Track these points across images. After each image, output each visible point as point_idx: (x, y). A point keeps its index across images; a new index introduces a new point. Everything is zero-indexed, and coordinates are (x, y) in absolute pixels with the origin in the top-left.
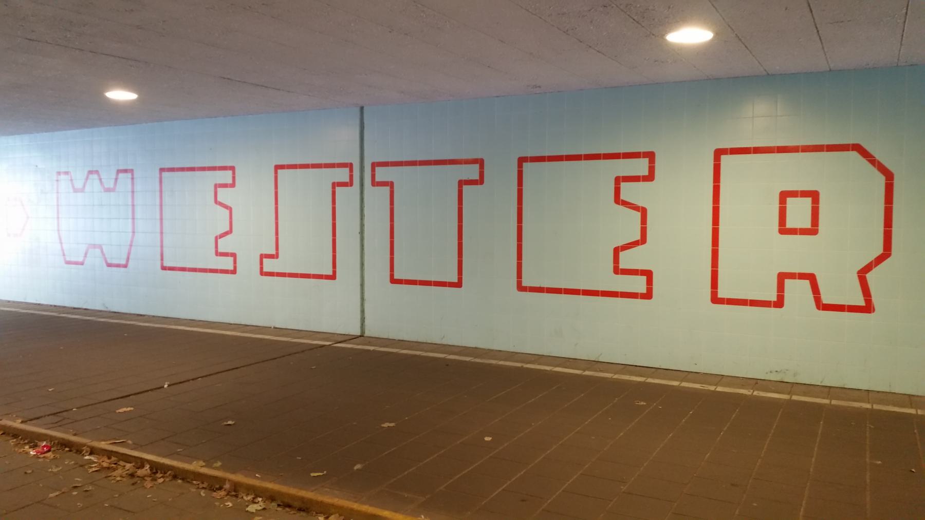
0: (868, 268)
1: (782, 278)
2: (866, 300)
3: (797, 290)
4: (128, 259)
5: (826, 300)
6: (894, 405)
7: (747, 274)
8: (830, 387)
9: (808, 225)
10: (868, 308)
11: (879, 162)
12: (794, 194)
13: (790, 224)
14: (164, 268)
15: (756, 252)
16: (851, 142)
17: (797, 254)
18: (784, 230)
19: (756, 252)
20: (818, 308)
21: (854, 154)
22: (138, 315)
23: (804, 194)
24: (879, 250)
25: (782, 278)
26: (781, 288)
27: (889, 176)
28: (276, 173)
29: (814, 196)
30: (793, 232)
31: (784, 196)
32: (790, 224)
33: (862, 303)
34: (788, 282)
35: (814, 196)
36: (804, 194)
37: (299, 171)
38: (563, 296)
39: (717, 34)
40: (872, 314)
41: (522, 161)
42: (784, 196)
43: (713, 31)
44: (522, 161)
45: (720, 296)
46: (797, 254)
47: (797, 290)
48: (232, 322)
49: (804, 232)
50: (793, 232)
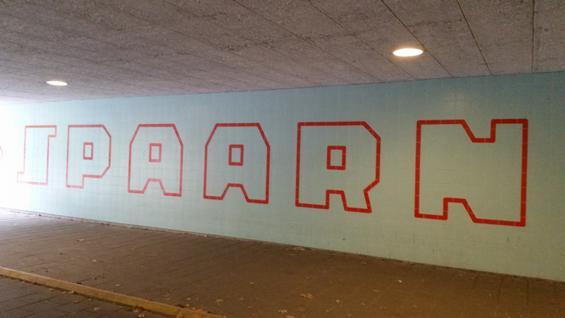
0: (368, 188)
1: (446, 201)
3: (335, 199)
4: (181, 189)
5: (349, 205)
7: (313, 193)
10: (369, 210)
13: (332, 164)
14: (130, 191)
16: (361, 120)
18: (330, 167)
20: (345, 210)
22: (447, 267)
25: (446, 201)
28: (69, 129)
31: (330, 148)
32: (332, 164)
33: (365, 207)
34: (450, 204)
38: (313, 209)
39: (391, 54)
41: (420, 123)
42: (330, 148)
43: (394, 55)
44: (300, 125)
47: (335, 199)
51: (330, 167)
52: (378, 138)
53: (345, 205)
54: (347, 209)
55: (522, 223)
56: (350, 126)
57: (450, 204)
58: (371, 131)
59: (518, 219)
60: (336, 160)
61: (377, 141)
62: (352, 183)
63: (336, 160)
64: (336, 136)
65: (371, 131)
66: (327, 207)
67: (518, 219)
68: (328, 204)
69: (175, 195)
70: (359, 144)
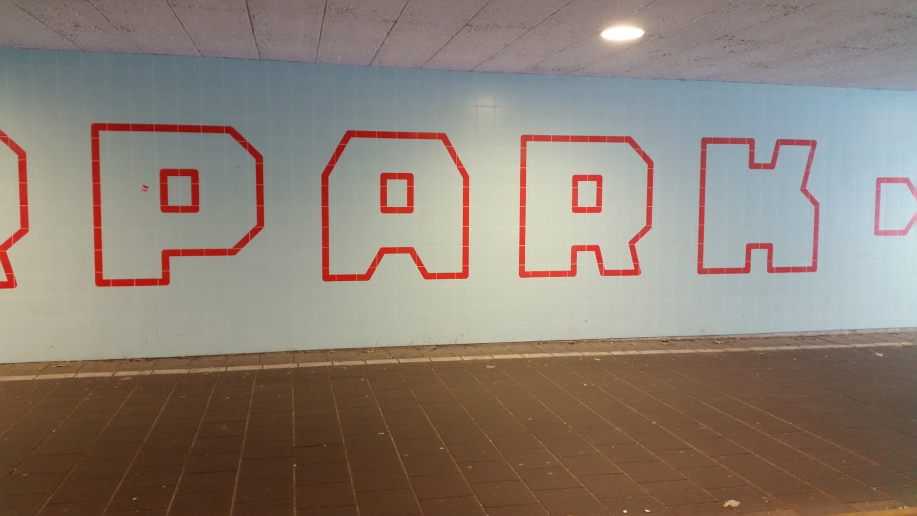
2: (7, 276)
3: (586, 260)
5: (607, 267)
6: (22, 375)
7: (547, 252)
8: (260, 354)
9: (189, 203)
11: (250, 146)
12: (174, 173)
13: (390, 204)
15: (555, 231)
16: (624, 135)
17: (587, 229)
18: (576, 209)
19: (555, 231)
20: (601, 274)
21: (627, 145)
23: (184, 173)
24: (17, 227)
26: (166, 265)
27: (22, 155)
29: (598, 179)
30: (175, 209)
31: (576, 179)
32: (390, 204)
35: (598, 179)
36: (184, 173)
37: (155, 134)
40: (15, 289)
41: (705, 141)
42: (576, 179)
43: (645, 29)
44: (705, 141)
45: (461, 271)
46: (587, 229)
47: (586, 260)
48: (183, 355)
49: (185, 209)
50: (175, 209)
51: (576, 209)
52: (650, 163)
53: (601, 267)
54: (605, 273)
55: (523, 274)
56: (202, 134)
57: (173, 260)
58: (245, 144)
59: (706, 265)
60: (587, 196)
61: (257, 161)
62: (611, 230)
63: (587, 196)
64: (586, 158)
65: (245, 144)
66: (573, 272)
67: (706, 265)
68: (574, 268)
69: (626, 273)
70: (620, 170)
